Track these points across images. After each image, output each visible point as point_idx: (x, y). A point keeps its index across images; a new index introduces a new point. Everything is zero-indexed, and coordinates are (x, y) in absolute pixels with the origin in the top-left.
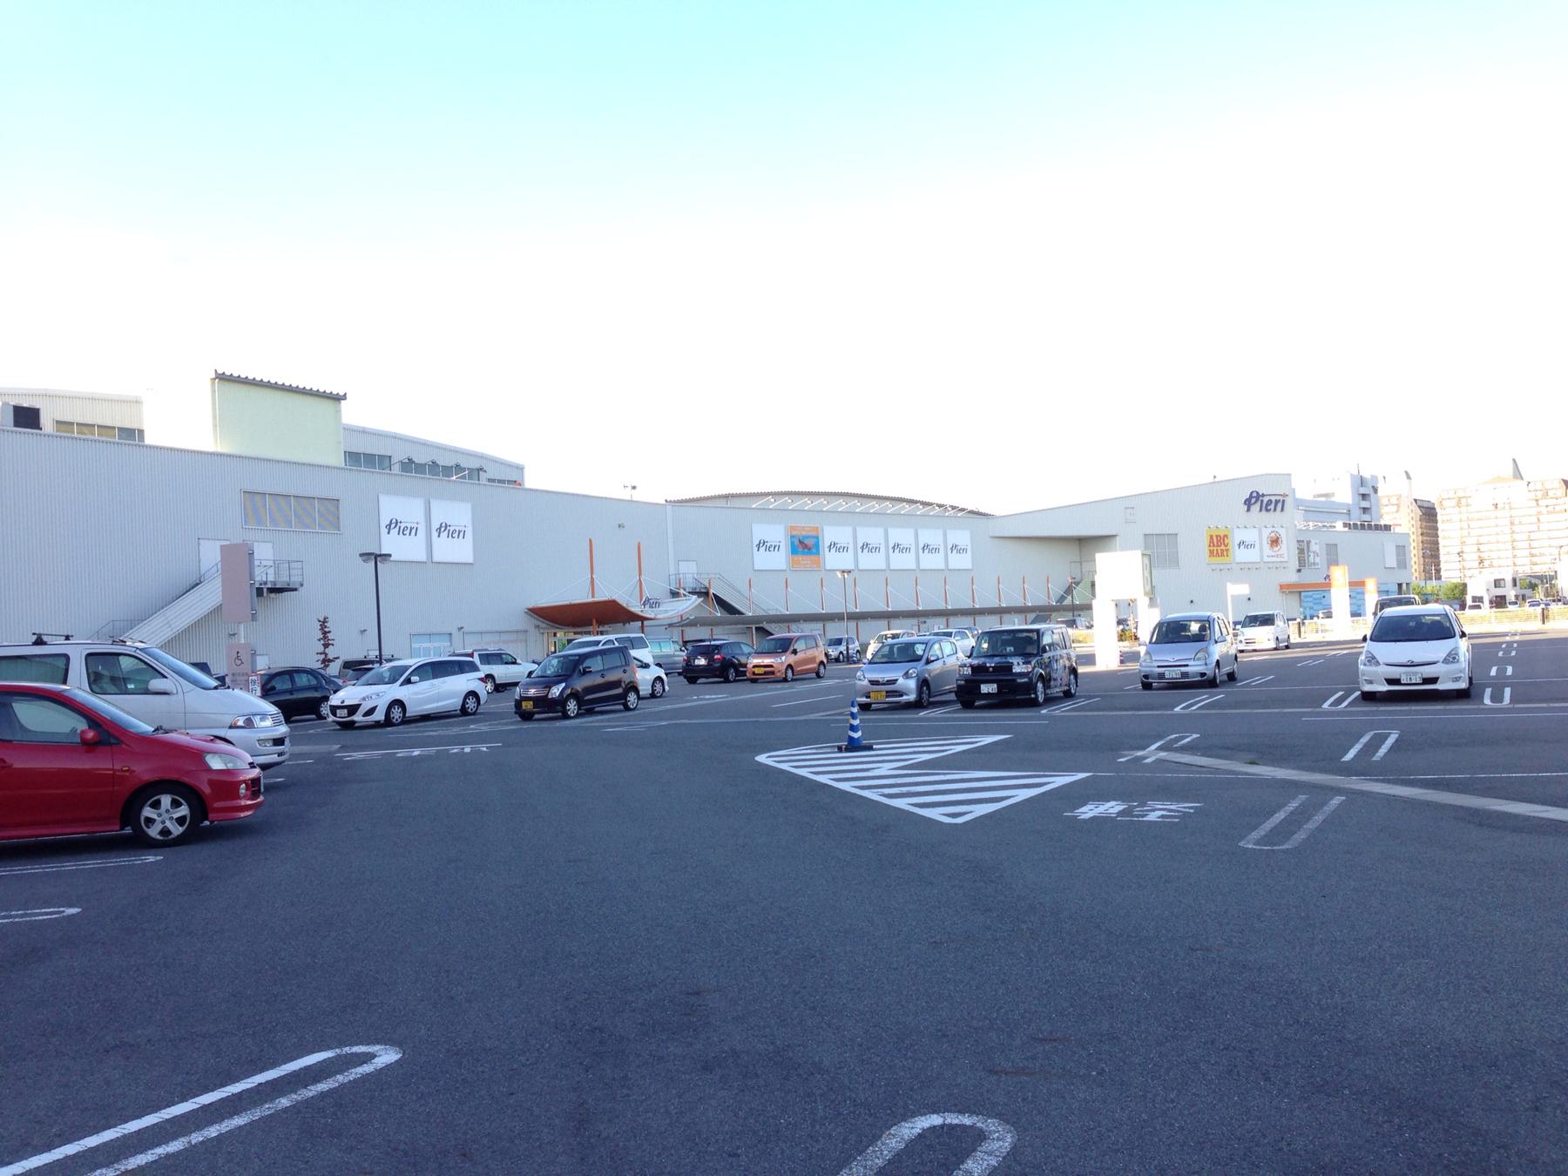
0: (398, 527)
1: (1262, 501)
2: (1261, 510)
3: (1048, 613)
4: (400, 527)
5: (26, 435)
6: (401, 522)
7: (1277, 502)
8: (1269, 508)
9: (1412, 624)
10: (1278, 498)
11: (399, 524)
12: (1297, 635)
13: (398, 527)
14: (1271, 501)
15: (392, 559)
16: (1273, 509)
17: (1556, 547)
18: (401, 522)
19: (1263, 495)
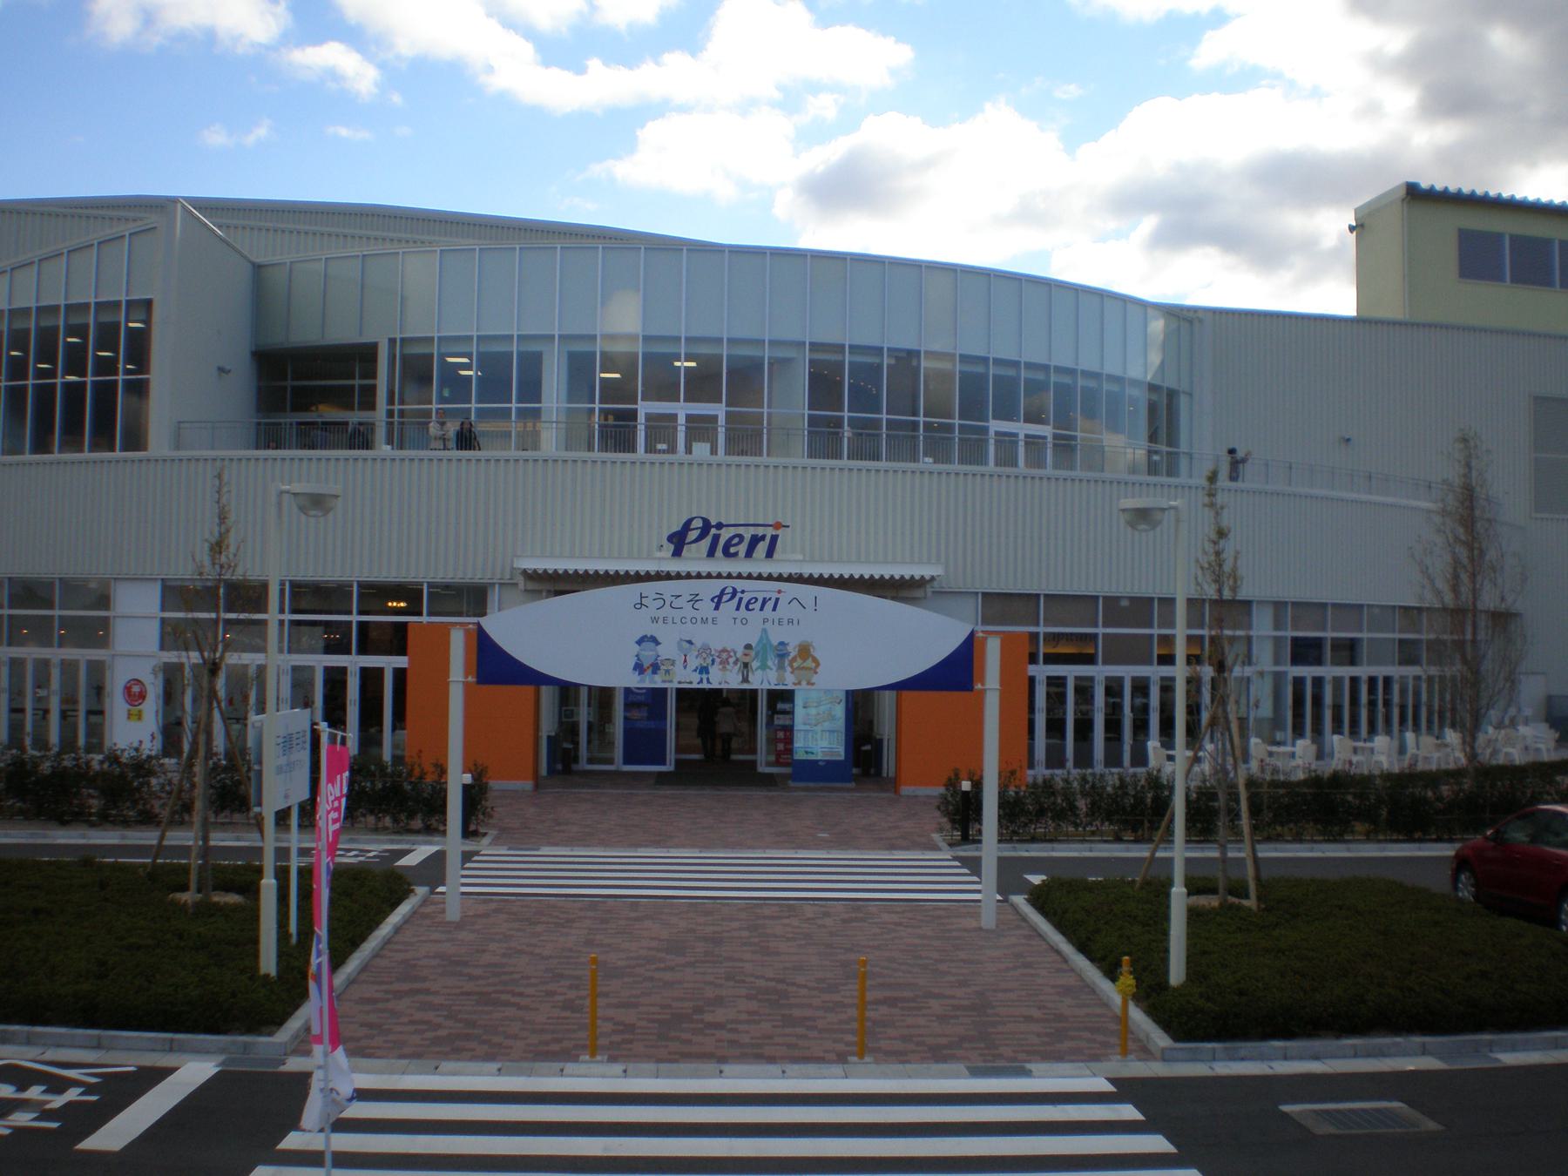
0: (736, 599)
1: (716, 538)
2: (738, 609)
3: (641, 286)
4: (741, 599)
5: (1122, 486)
6: (743, 592)
7: (755, 540)
8: (732, 550)
9: (1417, 835)
10: (760, 531)
11: (739, 595)
12: (787, 529)
13: (736, 599)
14: (741, 537)
15: (1149, 224)
16: (742, 553)
17: (1217, 570)
18: (743, 592)
19: (720, 526)
